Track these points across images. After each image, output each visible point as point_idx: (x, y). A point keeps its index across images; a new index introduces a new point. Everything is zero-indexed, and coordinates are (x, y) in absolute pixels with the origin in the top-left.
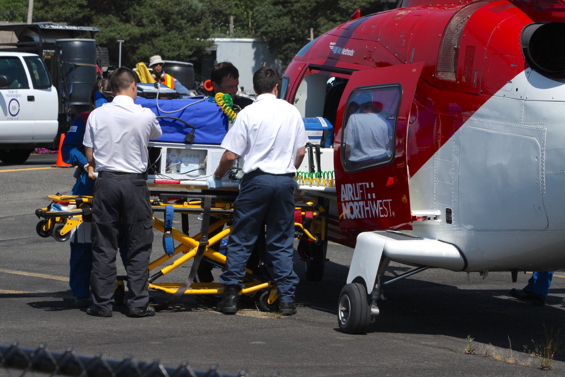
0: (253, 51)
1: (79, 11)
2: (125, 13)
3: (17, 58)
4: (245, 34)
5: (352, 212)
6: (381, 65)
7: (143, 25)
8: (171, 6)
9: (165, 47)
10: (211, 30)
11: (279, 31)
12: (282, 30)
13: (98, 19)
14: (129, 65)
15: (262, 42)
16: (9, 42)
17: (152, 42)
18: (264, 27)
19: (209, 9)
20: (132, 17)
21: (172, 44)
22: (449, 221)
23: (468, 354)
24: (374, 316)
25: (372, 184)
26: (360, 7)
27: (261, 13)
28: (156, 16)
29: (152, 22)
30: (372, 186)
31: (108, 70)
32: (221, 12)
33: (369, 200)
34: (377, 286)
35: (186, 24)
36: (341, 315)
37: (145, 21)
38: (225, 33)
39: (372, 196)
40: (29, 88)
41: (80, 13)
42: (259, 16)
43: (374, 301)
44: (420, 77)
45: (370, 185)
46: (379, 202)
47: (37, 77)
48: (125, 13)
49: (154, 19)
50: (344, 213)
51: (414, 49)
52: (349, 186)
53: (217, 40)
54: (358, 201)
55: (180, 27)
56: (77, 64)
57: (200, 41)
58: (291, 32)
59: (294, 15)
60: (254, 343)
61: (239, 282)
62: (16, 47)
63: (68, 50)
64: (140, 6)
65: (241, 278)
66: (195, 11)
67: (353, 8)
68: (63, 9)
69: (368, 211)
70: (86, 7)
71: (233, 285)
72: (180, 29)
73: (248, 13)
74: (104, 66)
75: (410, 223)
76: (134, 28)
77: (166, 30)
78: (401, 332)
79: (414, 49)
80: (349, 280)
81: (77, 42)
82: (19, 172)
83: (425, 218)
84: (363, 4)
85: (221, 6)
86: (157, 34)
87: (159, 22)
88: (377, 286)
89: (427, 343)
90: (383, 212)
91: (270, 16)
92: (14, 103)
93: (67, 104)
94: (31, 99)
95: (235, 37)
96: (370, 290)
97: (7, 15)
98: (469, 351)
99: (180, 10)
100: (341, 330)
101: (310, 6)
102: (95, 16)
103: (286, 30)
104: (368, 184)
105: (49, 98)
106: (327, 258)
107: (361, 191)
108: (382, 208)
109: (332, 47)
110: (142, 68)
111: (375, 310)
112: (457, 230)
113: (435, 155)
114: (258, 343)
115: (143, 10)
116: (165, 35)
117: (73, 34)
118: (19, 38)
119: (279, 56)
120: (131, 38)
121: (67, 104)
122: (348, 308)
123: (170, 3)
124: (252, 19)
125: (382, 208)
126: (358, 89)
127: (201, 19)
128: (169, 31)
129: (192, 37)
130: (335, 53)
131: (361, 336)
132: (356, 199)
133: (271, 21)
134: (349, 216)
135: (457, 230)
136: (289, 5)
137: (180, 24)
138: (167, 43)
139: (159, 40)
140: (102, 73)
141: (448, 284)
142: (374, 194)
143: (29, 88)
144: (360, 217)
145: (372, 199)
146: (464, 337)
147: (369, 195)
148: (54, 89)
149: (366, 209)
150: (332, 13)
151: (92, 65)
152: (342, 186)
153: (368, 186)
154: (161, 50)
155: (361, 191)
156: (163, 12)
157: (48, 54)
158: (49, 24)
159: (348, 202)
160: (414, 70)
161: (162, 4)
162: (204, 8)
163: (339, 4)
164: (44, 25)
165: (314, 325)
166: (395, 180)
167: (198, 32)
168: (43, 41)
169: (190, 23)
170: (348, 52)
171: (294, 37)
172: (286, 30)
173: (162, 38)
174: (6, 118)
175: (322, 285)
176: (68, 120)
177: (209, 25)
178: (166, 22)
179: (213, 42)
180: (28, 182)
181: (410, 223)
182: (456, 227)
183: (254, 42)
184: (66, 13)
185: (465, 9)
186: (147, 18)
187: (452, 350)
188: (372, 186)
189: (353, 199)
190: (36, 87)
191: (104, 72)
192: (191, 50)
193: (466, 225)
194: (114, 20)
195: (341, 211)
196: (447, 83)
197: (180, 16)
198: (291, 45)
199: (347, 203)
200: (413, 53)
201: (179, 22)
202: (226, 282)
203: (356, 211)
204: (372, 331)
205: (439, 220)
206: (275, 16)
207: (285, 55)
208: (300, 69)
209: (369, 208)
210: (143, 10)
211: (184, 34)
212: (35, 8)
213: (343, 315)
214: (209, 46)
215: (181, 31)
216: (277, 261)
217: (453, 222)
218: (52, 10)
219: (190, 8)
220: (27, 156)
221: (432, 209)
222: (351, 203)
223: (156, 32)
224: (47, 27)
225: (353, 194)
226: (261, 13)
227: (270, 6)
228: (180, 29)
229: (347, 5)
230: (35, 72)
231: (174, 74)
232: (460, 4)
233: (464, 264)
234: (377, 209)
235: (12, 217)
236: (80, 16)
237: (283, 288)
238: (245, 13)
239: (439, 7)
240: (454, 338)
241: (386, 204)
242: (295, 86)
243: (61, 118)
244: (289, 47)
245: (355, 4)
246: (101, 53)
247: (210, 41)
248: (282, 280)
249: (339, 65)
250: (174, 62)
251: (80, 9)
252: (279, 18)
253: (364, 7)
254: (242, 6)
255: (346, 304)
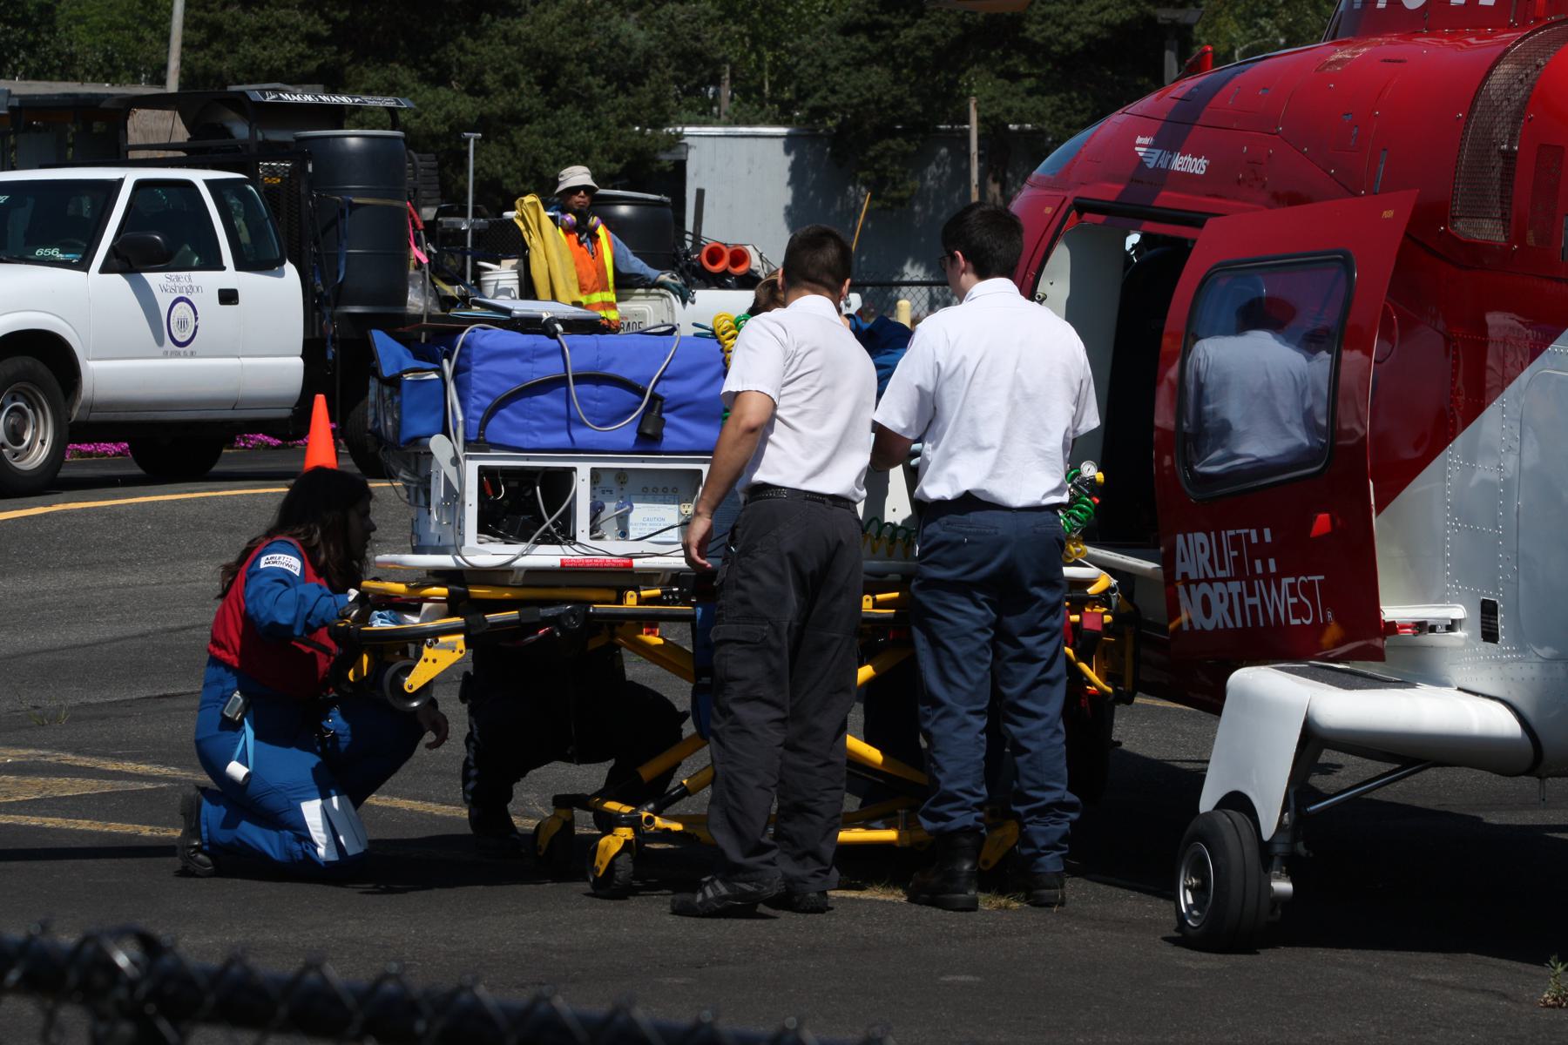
0: (787, 161)
1: (309, 52)
2: (434, 56)
3: (189, 185)
4: (763, 114)
5: (1207, 610)
6: (1294, 199)
7: (484, 92)
8: (562, 39)
9: (547, 151)
10: (673, 103)
11: (859, 105)
12: (867, 102)
13: (361, 73)
14: (497, 196)
15: (813, 137)
16: (164, 140)
17: (511, 138)
18: (818, 95)
19: (666, 47)
20: (455, 70)
21: (564, 142)
22: (1490, 635)
23: (1553, 1007)
24: (1280, 899)
25: (1267, 532)
26: (1083, 38)
27: (807, 56)
28: (520, 67)
29: (510, 82)
30: (1268, 538)
31: (437, 216)
32: (699, 55)
33: (1259, 577)
34: (1286, 819)
35: (604, 87)
36: (1186, 898)
37: (489, 79)
38: (706, 114)
39: (1265, 566)
40: (223, 269)
41: (309, 57)
42: (803, 63)
43: (1276, 861)
44: (1406, 234)
45: (1261, 535)
46: (1286, 581)
47: (245, 237)
48: (434, 56)
49: (515, 74)
50: (1184, 617)
51: (1384, 155)
52: (1201, 537)
53: (688, 130)
54: (1224, 580)
55: (586, 95)
56: (355, 201)
57: (642, 133)
58: (893, 107)
59: (901, 60)
60: (949, 978)
61: (977, 819)
62: (182, 154)
63: (330, 159)
64: (475, 40)
65: (979, 806)
66: (628, 51)
67: (1063, 39)
68: (265, 48)
69: (1253, 608)
70: (327, 41)
71: (965, 831)
72: (587, 103)
73: (760, 57)
74: (425, 205)
75: (1378, 642)
76: (459, 100)
77: (548, 104)
78: (1353, 947)
79: (1384, 155)
80: (1207, 803)
81: (353, 139)
82: (201, 501)
83: (1421, 627)
84: (1090, 29)
85: (697, 39)
86: (524, 115)
87: (529, 83)
88: (1286, 819)
89: (1432, 976)
90: (1299, 610)
91: (832, 63)
92: (182, 310)
93: (327, 311)
94: (228, 297)
95: (737, 123)
96: (1268, 829)
97: (97, 62)
98: (1555, 999)
99: (586, 50)
100: (1184, 938)
101: (944, 35)
102: (350, 68)
103: (878, 101)
104: (1253, 533)
105: (278, 295)
106: (1115, 738)
107: (1235, 553)
108: (1295, 600)
109: (1141, 151)
110: (532, 211)
111: (1283, 886)
112: (1513, 661)
113: (1448, 451)
114: (962, 978)
115: (483, 51)
116: (545, 117)
117: (337, 116)
118: (190, 127)
119: (861, 175)
120: (451, 127)
121: (327, 311)
122: (1205, 880)
123: (559, 29)
124: (771, 73)
125: (1295, 600)
126: (1224, 267)
127: (646, 75)
128: (557, 107)
129: (621, 124)
130: (1150, 166)
131: (1244, 959)
132: (1221, 574)
133: (837, 78)
134: (1201, 622)
135: (1513, 661)
136: (887, 32)
137: (588, 87)
138: (551, 141)
139: (530, 133)
140: (421, 226)
141: (1454, 810)
142: (1272, 562)
143: (223, 269)
144: (1230, 625)
145: (1266, 576)
146: (1541, 960)
147: (1258, 563)
148: (290, 269)
149: (1248, 601)
150: (1007, 56)
151: (397, 203)
152: (1180, 538)
153: (1254, 539)
154: (536, 160)
155: (1235, 553)
156: (540, 53)
157: (273, 172)
158: (275, 91)
159: (1197, 582)
160: (1388, 214)
161: (537, 34)
162: (652, 43)
163: (1025, 30)
164: (262, 92)
165: (1108, 930)
166: (1333, 520)
167: (638, 109)
168: (260, 135)
169: (615, 85)
170: (1190, 164)
171: (900, 120)
172: (878, 101)
173: (536, 127)
174: (160, 351)
175: (1144, 823)
176: (330, 357)
177: (667, 91)
178: (547, 83)
179: (680, 136)
180: (231, 530)
181: (1378, 642)
182: (1511, 652)
183: (788, 136)
184: (271, 58)
185: (1533, 41)
186: (496, 71)
187: (1504, 996)
188: (1268, 538)
189: (1211, 575)
190: (240, 266)
191: (426, 223)
192: (618, 160)
193: (1541, 646)
194: (405, 76)
195: (1174, 611)
196: (1476, 251)
197: (586, 66)
198: (892, 143)
199: (1192, 587)
200: (1382, 167)
201: (583, 82)
202: (941, 824)
203: (1220, 610)
204: (1272, 944)
205: (1460, 633)
206: (848, 65)
207: (876, 171)
208: (1048, 210)
209: (1256, 601)
210: (483, 51)
211: (600, 114)
212: (186, 45)
213: (1190, 901)
214: (668, 149)
215: (590, 108)
216: (1027, 756)
217: (1502, 637)
218: (232, 52)
219: (614, 43)
220: (215, 456)
221: (1442, 600)
222: (1204, 587)
223: (523, 110)
224: (271, 98)
225: (1211, 561)
226: (807, 56)
227: (834, 36)
228: (587, 103)
229: (1047, 34)
230: (239, 222)
231: (615, 225)
232: (1510, 28)
233: (1528, 758)
234: (1281, 601)
235: (201, 626)
236: (312, 65)
237: (1044, 834)
238: (754, 56)
239: (1449, 37)
240: (1505, 963)
241: (1308, 589)
242: (1037, 258)
243: (311, 350)
244: (889, 148)
245: (1067, 29)
246: (420, 165)
247: (669, 134)
248: (1042, 812)
249: (1167, 198)
250: (619, 192)
251: (310, 47)
252: (859, 70)
253: (1091, 37)
254: (742, 36)
255: (1199, 869)
